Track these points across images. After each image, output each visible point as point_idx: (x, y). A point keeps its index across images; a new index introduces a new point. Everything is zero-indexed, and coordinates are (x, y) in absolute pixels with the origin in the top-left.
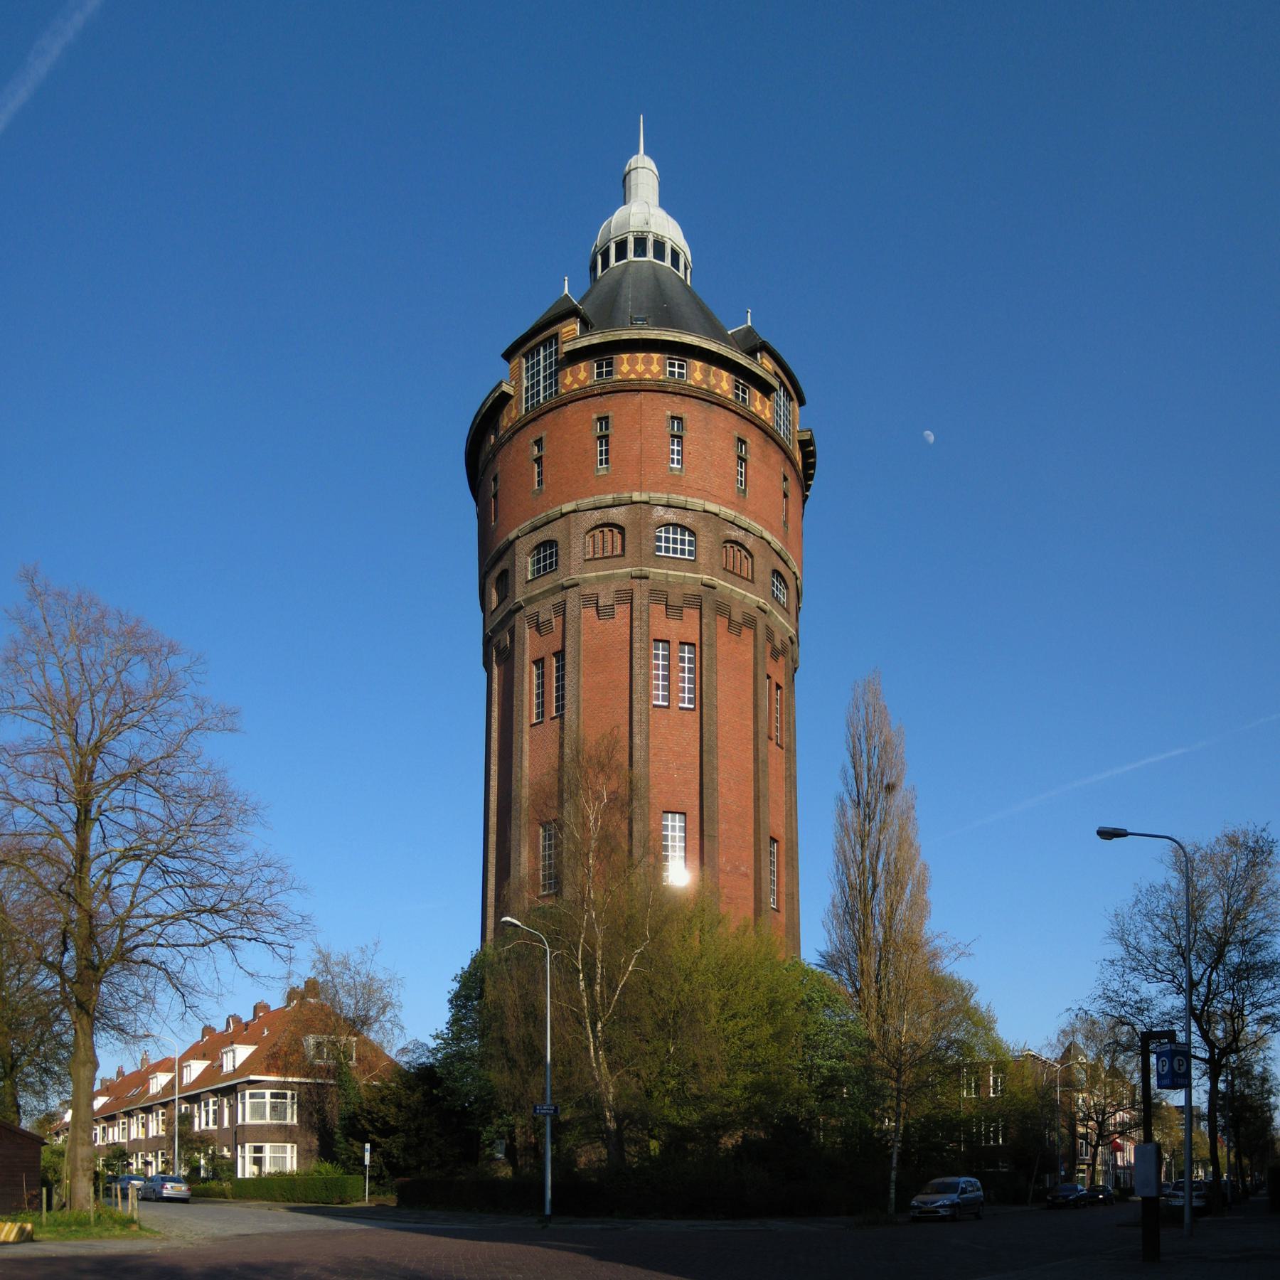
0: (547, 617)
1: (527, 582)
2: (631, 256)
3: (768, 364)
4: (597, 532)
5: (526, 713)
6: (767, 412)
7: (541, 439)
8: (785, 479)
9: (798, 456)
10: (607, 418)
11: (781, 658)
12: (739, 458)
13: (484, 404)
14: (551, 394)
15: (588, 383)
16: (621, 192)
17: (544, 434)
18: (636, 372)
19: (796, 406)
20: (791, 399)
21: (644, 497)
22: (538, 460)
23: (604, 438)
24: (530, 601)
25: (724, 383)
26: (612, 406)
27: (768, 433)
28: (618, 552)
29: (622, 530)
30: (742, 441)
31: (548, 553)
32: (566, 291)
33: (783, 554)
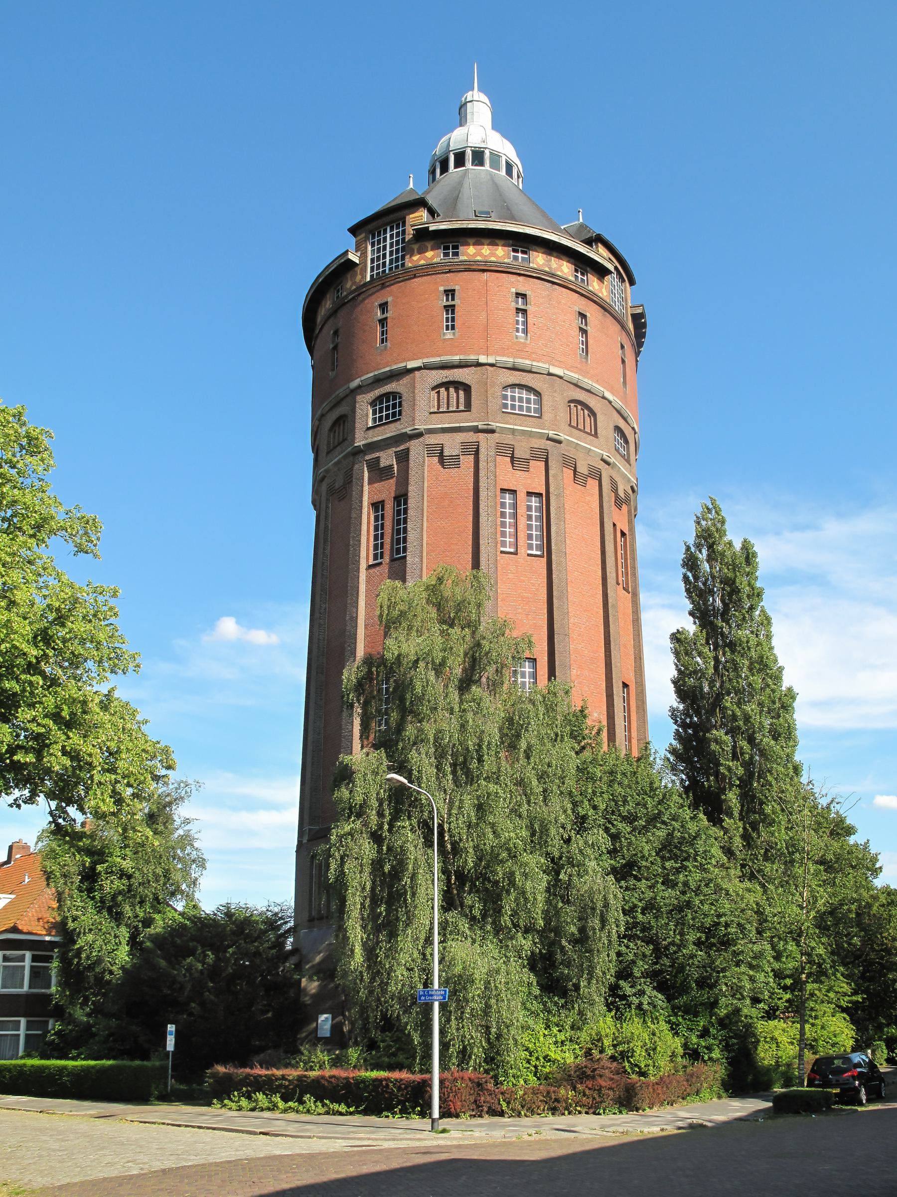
0: (388, 463)
1: (369, 429)
2: (469, 164)
3: (602, 250)
4: (442, 390)
5: (363, 553)
6: (604, 290)
7: (386, 303)
8: (622, 347)
9: (631, 326)
10: (454, 290)
11: (624, 507)
12: (581, 329)
13: (328, 267)
14: (397, 267)
15: (435, 260)
16: (461, 116)
17: (390, 299)
18: (481, 255)
19: (628, 285)
20: (623, 281)
21: (491, 360)
22: (383, 322)
23: (450, 309)
24: (372, 447)
25: (565, 269)
26: (456, 281)
27: (605, 308)
28: (462, 408)
29: (467, 388)
30: (583, 316)
31: (391, 406)
32: (411, 186)
33: (623, 412)
